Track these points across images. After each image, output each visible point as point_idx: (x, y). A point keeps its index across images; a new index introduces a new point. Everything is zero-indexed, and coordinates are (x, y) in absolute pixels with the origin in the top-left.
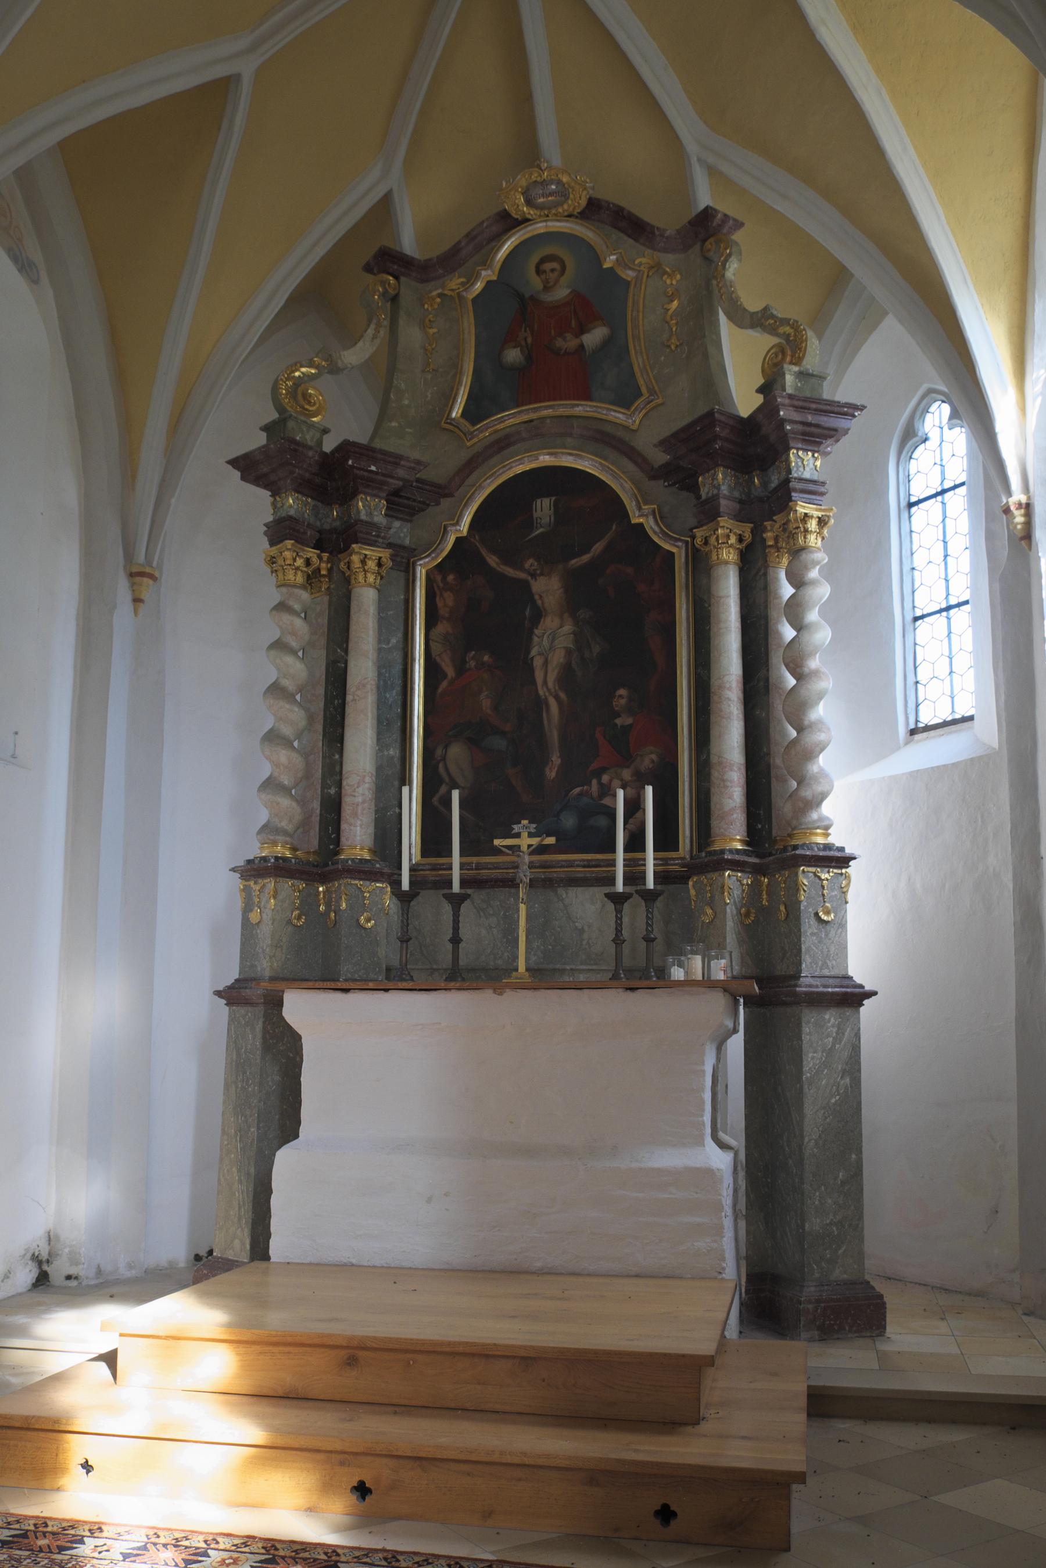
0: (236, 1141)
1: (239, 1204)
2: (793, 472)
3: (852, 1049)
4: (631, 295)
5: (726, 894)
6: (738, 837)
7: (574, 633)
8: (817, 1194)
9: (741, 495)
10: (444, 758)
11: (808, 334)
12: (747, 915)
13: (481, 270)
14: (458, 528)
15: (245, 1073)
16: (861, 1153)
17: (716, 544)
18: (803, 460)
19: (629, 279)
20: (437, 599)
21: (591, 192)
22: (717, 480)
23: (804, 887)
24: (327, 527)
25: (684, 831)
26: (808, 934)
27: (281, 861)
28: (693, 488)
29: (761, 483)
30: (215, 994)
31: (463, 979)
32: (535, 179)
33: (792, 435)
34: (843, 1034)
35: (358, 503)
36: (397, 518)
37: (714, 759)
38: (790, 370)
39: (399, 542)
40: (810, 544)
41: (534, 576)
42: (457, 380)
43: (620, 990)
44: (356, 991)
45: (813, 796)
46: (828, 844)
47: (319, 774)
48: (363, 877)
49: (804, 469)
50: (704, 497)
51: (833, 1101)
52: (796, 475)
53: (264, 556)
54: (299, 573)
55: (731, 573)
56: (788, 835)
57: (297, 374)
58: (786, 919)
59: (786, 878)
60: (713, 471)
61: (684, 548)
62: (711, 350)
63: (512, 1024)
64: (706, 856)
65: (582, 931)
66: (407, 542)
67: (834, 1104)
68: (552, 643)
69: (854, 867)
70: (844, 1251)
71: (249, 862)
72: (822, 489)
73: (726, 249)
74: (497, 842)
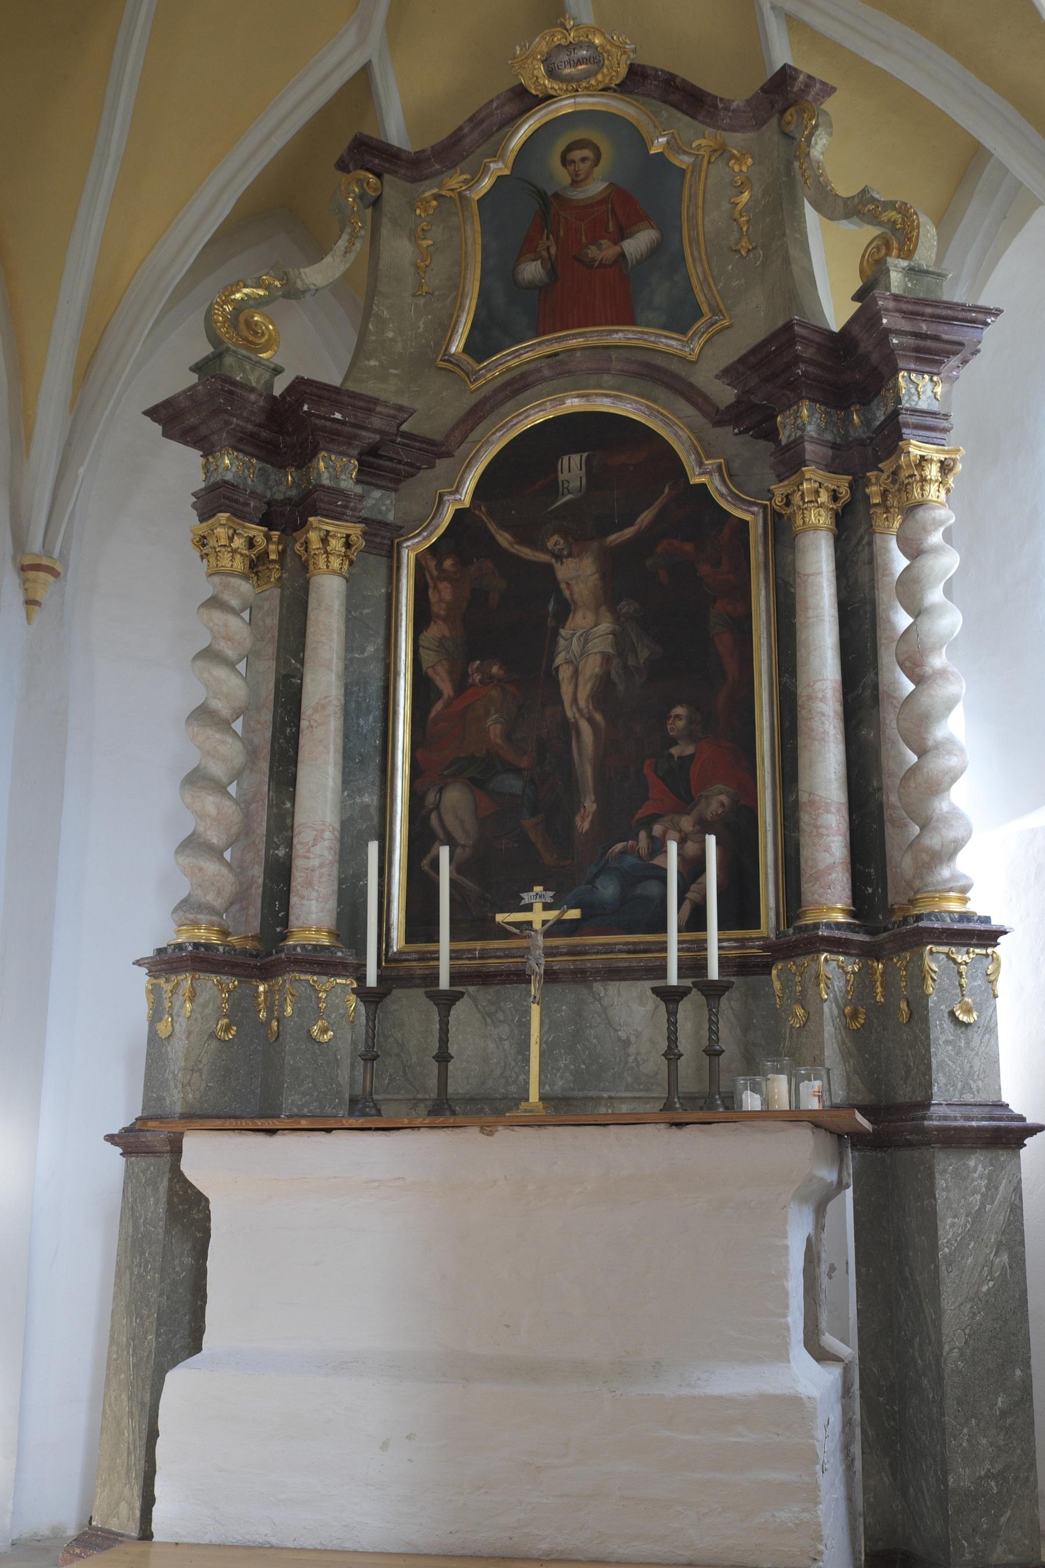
0: (128, 1352)
1: (129, 1448)
2: (903, 402)
3: (1011, 1211)
4: (686, 186)
5: (822, 985)
6: (839, 906)
7: (613, 633)
8: (965, 1431)
9: (835, 438)
10: (437, 807)
11: (921, 220)
12: (854, 1016)
13: (490, 162)
14: (458, 497)
15: (142, 1253)
16: (1029, 1367)
17: (801, 503)
18: (918, 385)
19: (684, 167)
20: (430, 591)
21: (632, 56)
22: (801, 418)
23: (933, 975)
24: (279, 496)
25: (767, 900)
26: (941, 1043)
27: (203, 949)
28: (771, 434)
29: (861, 422)
30: (107, 1140)
31: (454, 1113)
32: (559, 42)
33: (901, 352)
34: (997, 1189)
35: (318, 464)
36: (378, 487)
37: (804, 798)
38: (895, 266)
39: (380, 517)
40: (930, 497)
41: (559, 557)
42: (458, 305)
43: (662, 1126)
44: (286, 1132)
45: (943, 846)
46: (965, 913)
47: (263, 829)
48: (318, 970)
49: (919, 398)
50: (784, 441)
51: (985, 1289)
52: (907, 405)
53: (191, 535)
54: (238, 557)
55: (823, 542)
56: (909, 901)
57: (238, 296)
58: (908, 1022)
59: (908, 962)
60: (796, 407)
61: (761, 515)
62: (794, 252)
63: (506, 1179)
64: (794, 934)
65: (627, 1043)
66: (391, 517)
67: (986, 1294)
68: (584, 647)
69: (1004, 947)
70: (1009, 1519)
71: (160, 951)
72: (945, 424)
73: (811, 119)
74: (500, 918)
